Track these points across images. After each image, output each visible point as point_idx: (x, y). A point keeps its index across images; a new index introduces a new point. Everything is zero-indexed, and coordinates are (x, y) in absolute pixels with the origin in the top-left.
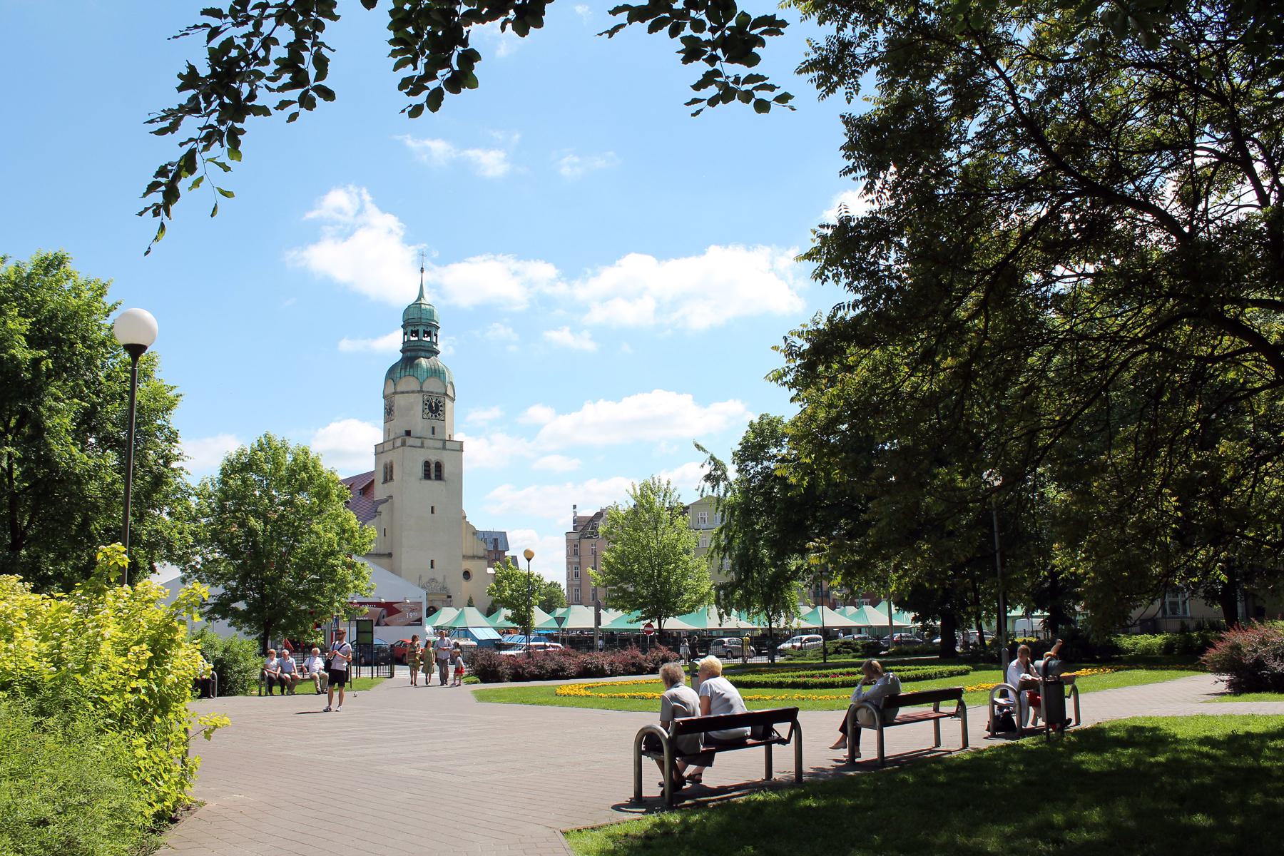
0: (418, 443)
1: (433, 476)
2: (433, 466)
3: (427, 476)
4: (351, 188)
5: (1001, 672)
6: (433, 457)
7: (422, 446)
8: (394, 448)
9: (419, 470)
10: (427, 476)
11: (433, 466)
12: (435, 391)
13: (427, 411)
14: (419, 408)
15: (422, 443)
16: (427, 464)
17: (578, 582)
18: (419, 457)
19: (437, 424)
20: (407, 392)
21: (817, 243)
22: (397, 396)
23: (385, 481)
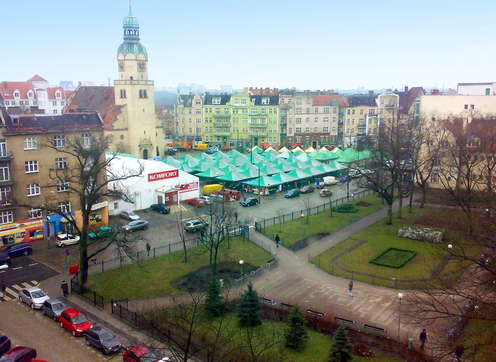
0: (136, 83)
1: (143, 97)
2: (143, 92)
3: (141, 97)
4: (325, 319)
5: (109, 215)
6: (143, 88)
7: (138, 84)
8: (318, 207)
9: (138, 95)
10: (141, 97)
11: (143, 92)
12: (142, 59)
13: (139, 68)
14: (136, 67)
15: (138, 83)
16: (141, 91)
17: (183, 125)
18: (138, 88)
19: (143, 73)
20: (130, 60)
21: (191, 303)
22: (126, 62)
23: (122, 97)
